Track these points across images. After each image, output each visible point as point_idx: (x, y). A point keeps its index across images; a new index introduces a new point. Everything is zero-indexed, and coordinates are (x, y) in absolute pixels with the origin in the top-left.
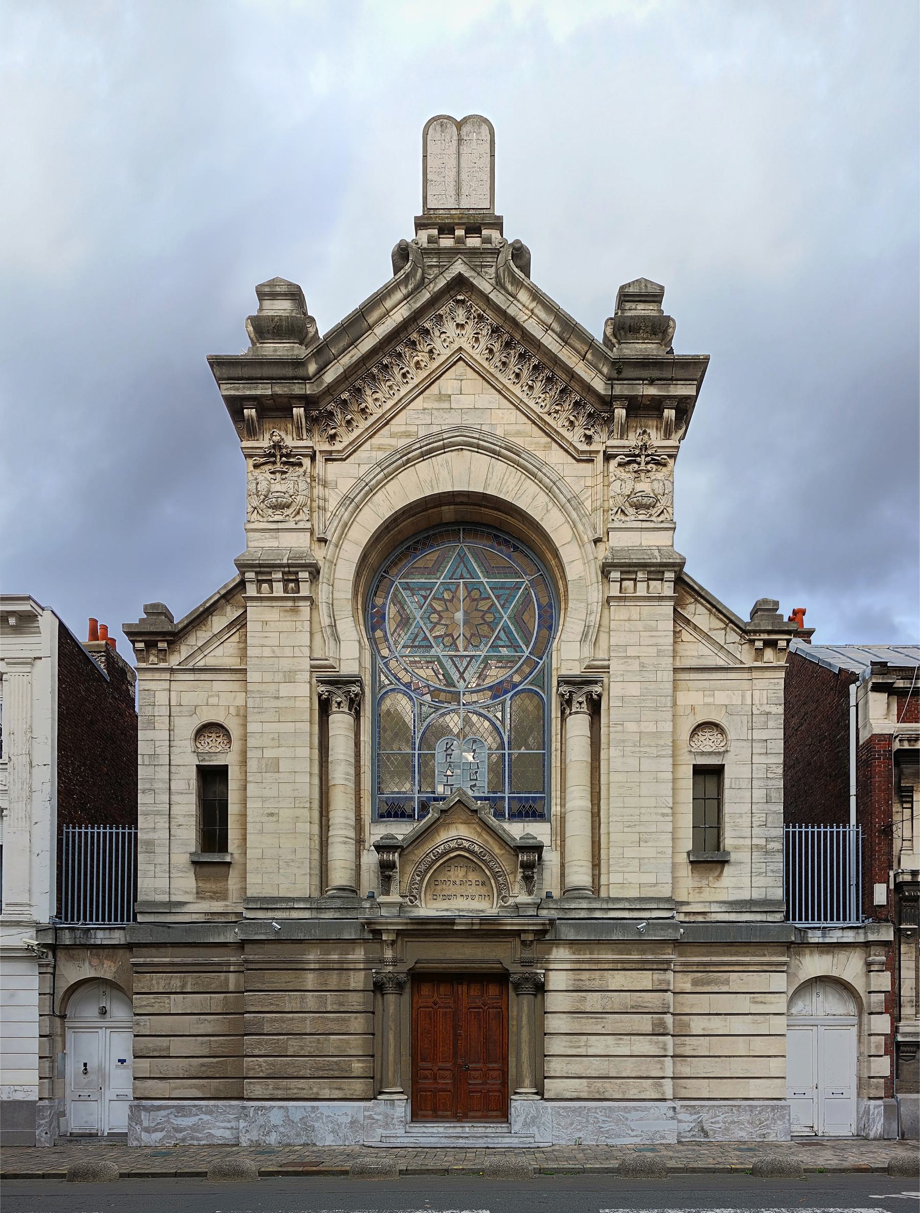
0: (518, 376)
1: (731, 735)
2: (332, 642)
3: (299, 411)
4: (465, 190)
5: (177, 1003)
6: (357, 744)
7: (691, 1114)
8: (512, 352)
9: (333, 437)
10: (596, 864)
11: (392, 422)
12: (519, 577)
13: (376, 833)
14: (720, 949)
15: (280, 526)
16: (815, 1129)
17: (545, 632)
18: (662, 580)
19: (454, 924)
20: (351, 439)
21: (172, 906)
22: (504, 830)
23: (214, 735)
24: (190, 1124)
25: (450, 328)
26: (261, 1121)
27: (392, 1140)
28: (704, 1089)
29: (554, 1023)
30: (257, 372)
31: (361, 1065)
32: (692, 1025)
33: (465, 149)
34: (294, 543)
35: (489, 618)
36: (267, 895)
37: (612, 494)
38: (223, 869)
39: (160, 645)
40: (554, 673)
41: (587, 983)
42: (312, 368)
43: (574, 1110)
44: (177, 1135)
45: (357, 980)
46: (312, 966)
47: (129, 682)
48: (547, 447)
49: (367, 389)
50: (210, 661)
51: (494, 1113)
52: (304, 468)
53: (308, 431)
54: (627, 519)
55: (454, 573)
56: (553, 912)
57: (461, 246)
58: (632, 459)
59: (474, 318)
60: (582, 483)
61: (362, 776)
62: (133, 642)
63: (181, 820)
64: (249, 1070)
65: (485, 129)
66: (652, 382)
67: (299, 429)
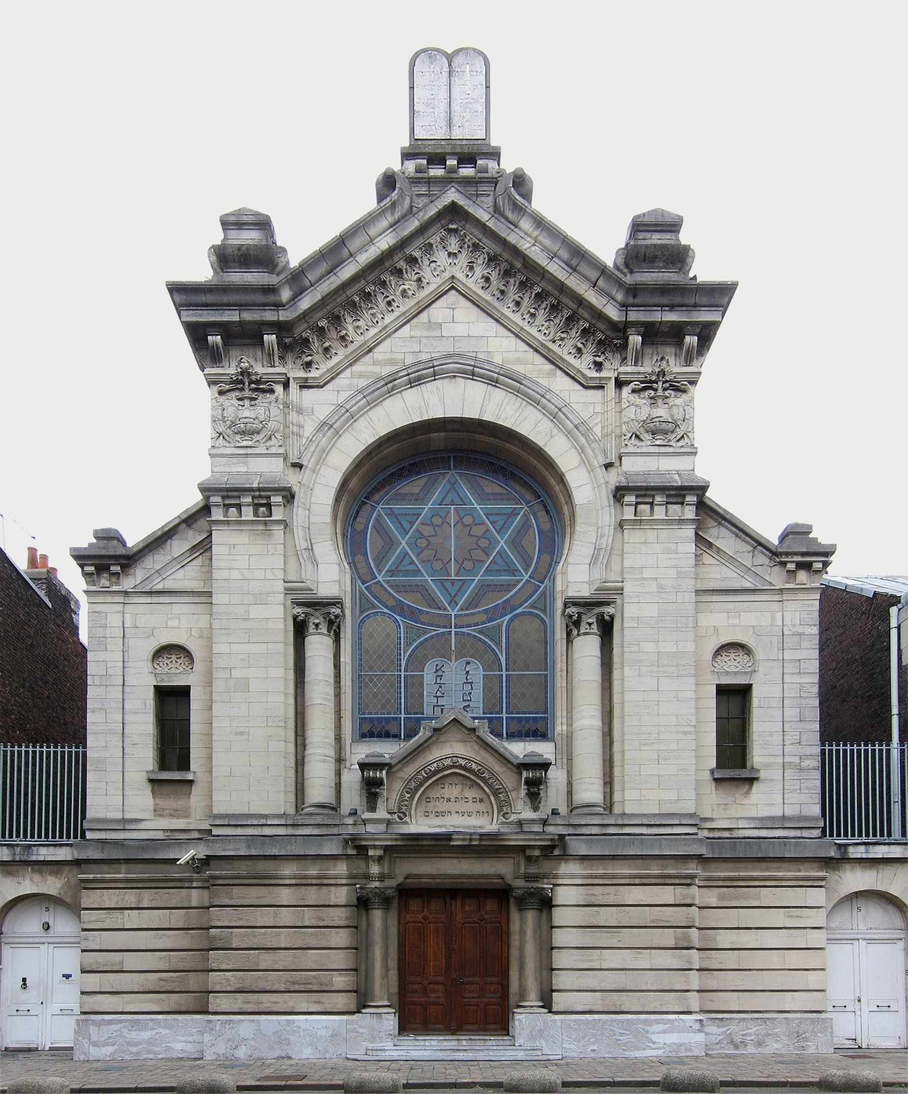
0: (518, 304)
1: (760, 654)
2: (309, 566)
3: (270, 339)
4: (456, 121)
5: (132, 919)
6: (337, 666)
7: (719, 1027)
8: (512, 281)
9: (308, 365)
10: (609, 782)
11: (376, 350)
12: (517, 504)
13: (361, 752)
14: (750, 865)
15: (249, 451)
16: (859, 1041)
17: (546, 557)
18: (682, 503)
19: (451, 840)
20: (329, 366)
21: (125, 823)
22: (506, 749)
23: (174, 657)
24: (146, 1038)
25: (441, 257)
26: (229, 1034)
27: (379, 1053)
28: (733, 1002)
29: (560, 938)
30: (225, 299)
31: (344, 979)
32: (719, 938)
33: (456, 80)
34: (264, 468)
35: (483, 543)
36: (236, 812)
37: (626, 420)
38: (184, 788)
39: (112, 568)
40: (559, 596)
41: (601, 898)
42: (286, 294)
43: (587, 1023)
44: (130, 1049)
45: (341, 895)
46: (288, 882)
47: (72, 610)
48: (550, 375)
49: (347, 316)
50: (169, 584)
51: (493, 1027)
52: (276, 394)
53: (281, 358)
54: (642, 444)
55: (443, 499)
56: (560, 828)
57: (454, 175)
58: (648, 385)
59: (469, 247)
60: (591, 409)
61: (343, 696)
62: (82, 566)
63: (136, 739)
64: (215, 984)
65: (480, 65)
66: (672, 307)
67: (271, 355)
